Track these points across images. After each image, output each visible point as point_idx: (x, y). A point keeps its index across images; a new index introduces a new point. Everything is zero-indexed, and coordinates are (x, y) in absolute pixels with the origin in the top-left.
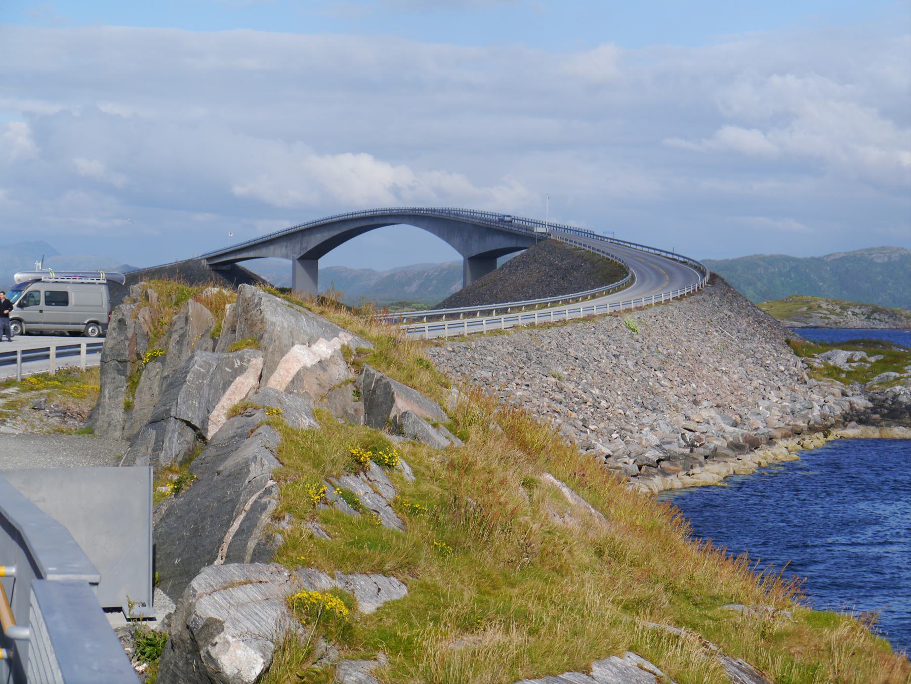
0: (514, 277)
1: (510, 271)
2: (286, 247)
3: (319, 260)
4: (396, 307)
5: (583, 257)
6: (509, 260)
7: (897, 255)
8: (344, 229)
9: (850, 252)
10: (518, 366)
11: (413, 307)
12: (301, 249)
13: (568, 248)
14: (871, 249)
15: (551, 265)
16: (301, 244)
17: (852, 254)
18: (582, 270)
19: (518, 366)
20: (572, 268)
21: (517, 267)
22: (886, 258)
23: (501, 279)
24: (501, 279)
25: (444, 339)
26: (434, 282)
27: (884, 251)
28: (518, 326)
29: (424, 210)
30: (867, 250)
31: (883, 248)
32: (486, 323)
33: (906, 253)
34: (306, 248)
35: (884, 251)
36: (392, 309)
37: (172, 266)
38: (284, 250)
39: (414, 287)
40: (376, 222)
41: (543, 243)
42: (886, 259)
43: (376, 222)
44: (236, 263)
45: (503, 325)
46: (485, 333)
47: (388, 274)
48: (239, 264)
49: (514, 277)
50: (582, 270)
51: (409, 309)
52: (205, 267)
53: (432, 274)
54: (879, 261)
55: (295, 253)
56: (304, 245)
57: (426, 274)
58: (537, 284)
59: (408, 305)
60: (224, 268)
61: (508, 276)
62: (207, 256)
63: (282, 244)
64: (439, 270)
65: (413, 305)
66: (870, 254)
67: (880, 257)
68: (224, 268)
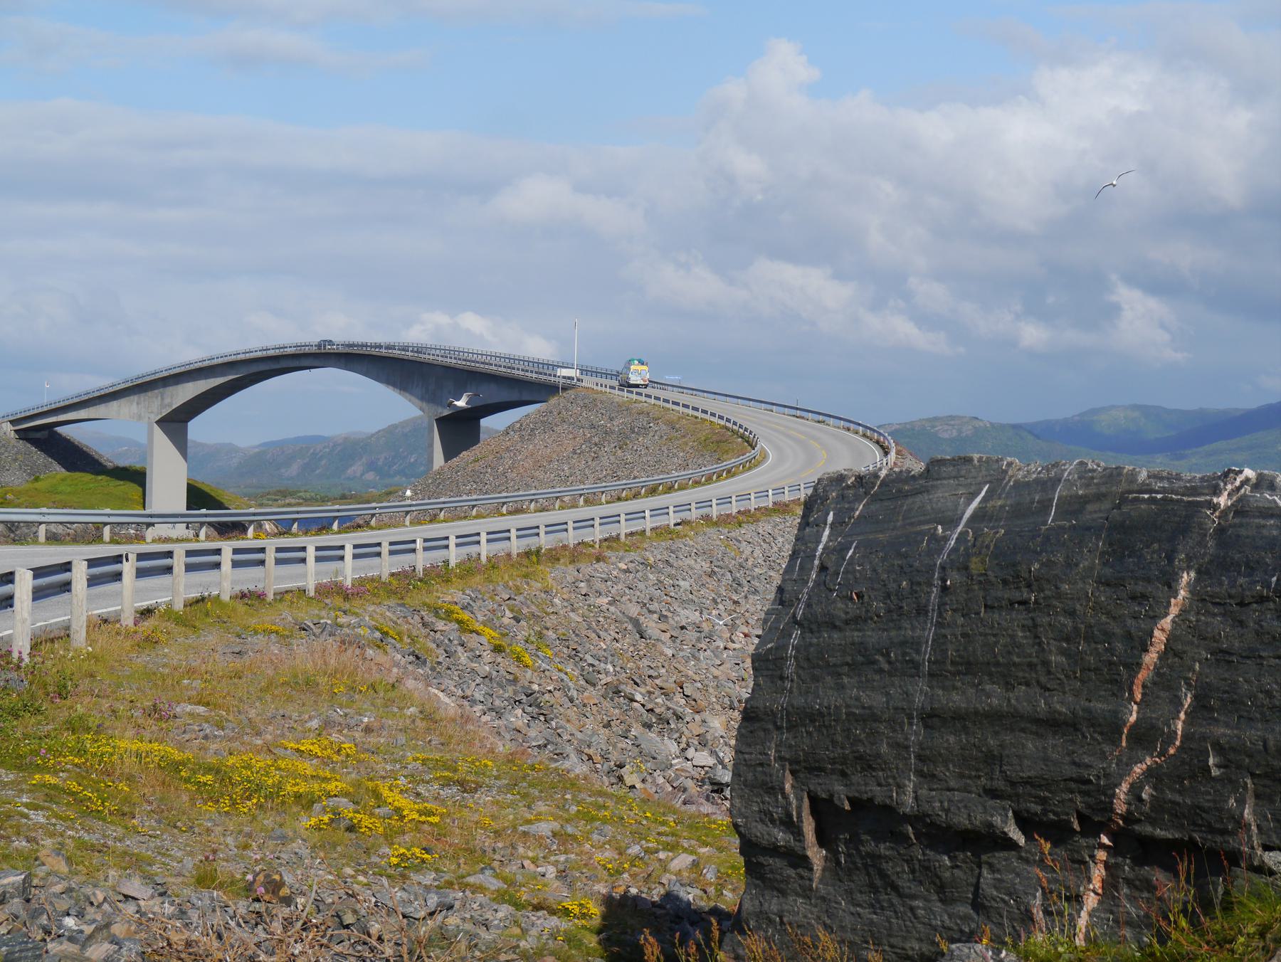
0: (531, 447)
1: (522, 437)
2: (138, 404)
3: (190, 424)
4: (274, 497)
5: (648, 414)
6: (517, 419)
7: (970, 427)
8: (254, 369)
9: (906, 423)
10: (730, 599)
11: (300, 498)
12: (163, 406)
13: (617, 400)
14: (936, 419)
15: (593, 426)
16: (162, 399)
17: (908, 426)
18: (651, 434)
19: (730, 599)
20: (633, 432)
21: (532, 430)
22: (954, 431)
23: (508, 449)
24: (508, 449)
25: (592, 546)
26: (323, 462)
27: (952, 422)
28: (689, 522)
29: (367, 346)
30: (929, 420)
31: (952, 418)
32: (651, 516)
33: (981, 424)
34: (170, 405)
35: (952, 422)
36: (268, 500)
37: (400, 390)
38: (134, 408)
39: (294, 469)
40: (283, 364)
41: (571, 393)
42: (955, 433)
43: (283, 364)
44: (56, 429)
45: (648, 524)
46: (648, 533)
47: (257, 450)
48: (59, 429)
49: (531, 447)
50: (651, 434)
51: (293, 501)
52: (8, 434)
53: (321, 451)
54: (946, 436)
55: (152, 412)
56: (167, 400)
57: (312, 451)
58: (576, 456)
59: (292, 494)
60: (38, 435)
61: (520, 444)
62: (11, 418)
63: (132, 397)
64: (331, 444)
65: (299, 494)
66: (933, 427)
67: (947, 430)
68: (38, 435)
